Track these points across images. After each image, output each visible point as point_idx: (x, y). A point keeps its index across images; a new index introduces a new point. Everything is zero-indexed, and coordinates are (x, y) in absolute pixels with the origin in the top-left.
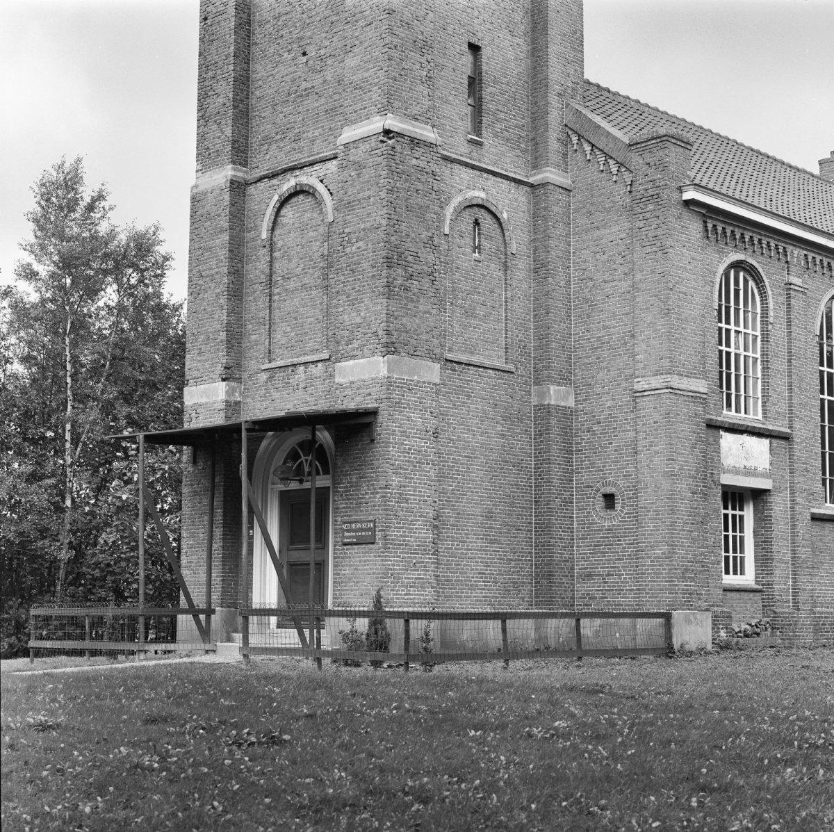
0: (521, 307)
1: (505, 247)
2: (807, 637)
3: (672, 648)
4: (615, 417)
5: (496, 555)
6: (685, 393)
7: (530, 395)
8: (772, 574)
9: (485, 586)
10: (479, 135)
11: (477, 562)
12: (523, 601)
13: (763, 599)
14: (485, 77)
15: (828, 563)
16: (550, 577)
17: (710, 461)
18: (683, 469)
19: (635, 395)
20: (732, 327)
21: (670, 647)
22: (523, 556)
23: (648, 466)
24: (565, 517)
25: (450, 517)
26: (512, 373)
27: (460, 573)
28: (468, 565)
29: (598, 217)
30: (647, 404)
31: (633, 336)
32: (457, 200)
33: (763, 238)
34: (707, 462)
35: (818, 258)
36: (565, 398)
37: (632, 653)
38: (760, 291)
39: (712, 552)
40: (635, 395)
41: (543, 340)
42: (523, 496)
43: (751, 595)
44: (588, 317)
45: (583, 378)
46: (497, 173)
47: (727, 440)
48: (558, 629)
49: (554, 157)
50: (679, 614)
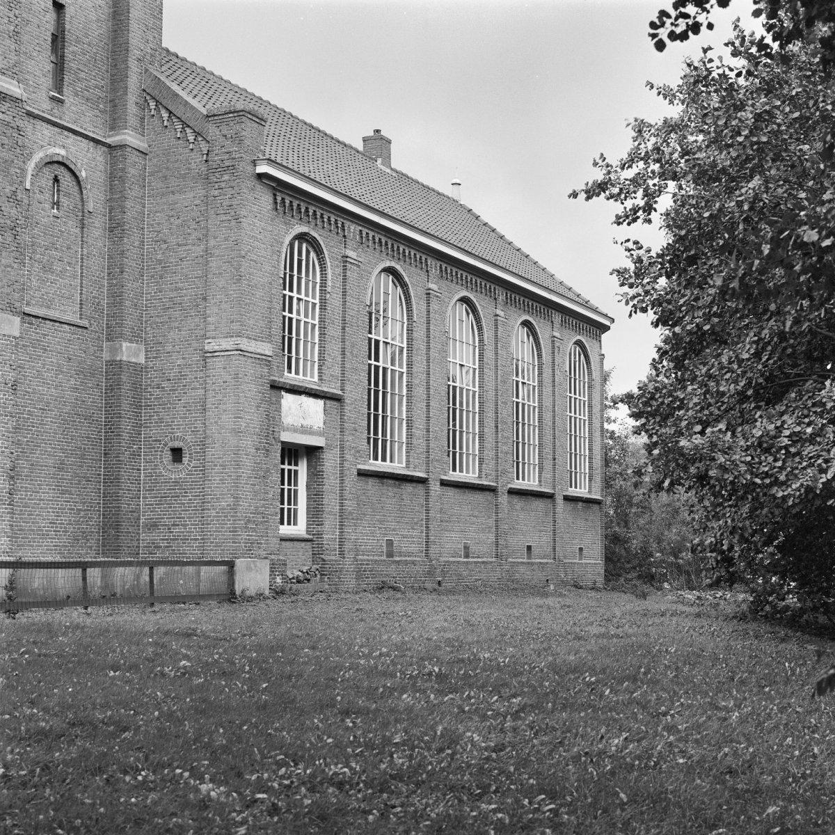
0: (97, 265)
1: (83, 205)
2: (350, 582)
3: (235, 594)
4: (185, 375)
5: (66, 505)
6: (252, 355)
7: (102, 350)
8: (322, 525)
9: (56, 535)
10: (60, 92)
11: (48, 512)
12: (91, 550)
13: (313, 547)
14: (68, 36)
15: (371, 515)
16: (117, 526)
17: (272, 418)
18: (249, 427)
19: (206, 355)
20: (295, 294)
21: (233, 593)
22: (92, 507)
23: (215, 422)
24: (133, 469)
25: (24, 468)
26: (86, 328)
27: (33, 523)
28: (39, 515)
29: (173, 182)
30: (217, 364)
31: (205, 299)
32: (38, 156)
33: (325, 213)
34: (269, 421)
35: (371, 234)
36: (136, 355)
37: (197, 598)
38: (320, 262)
39: (271, 504)
40: (206, 355)
41: (116, 297)
42: (93, 449)
43: (303, 544)
44: (161, 277)
45: (154, 337)
46: (77, 131)
47: (288, 400)
48: (123, 576)
49: (132, 120)
50: (241, 562)
